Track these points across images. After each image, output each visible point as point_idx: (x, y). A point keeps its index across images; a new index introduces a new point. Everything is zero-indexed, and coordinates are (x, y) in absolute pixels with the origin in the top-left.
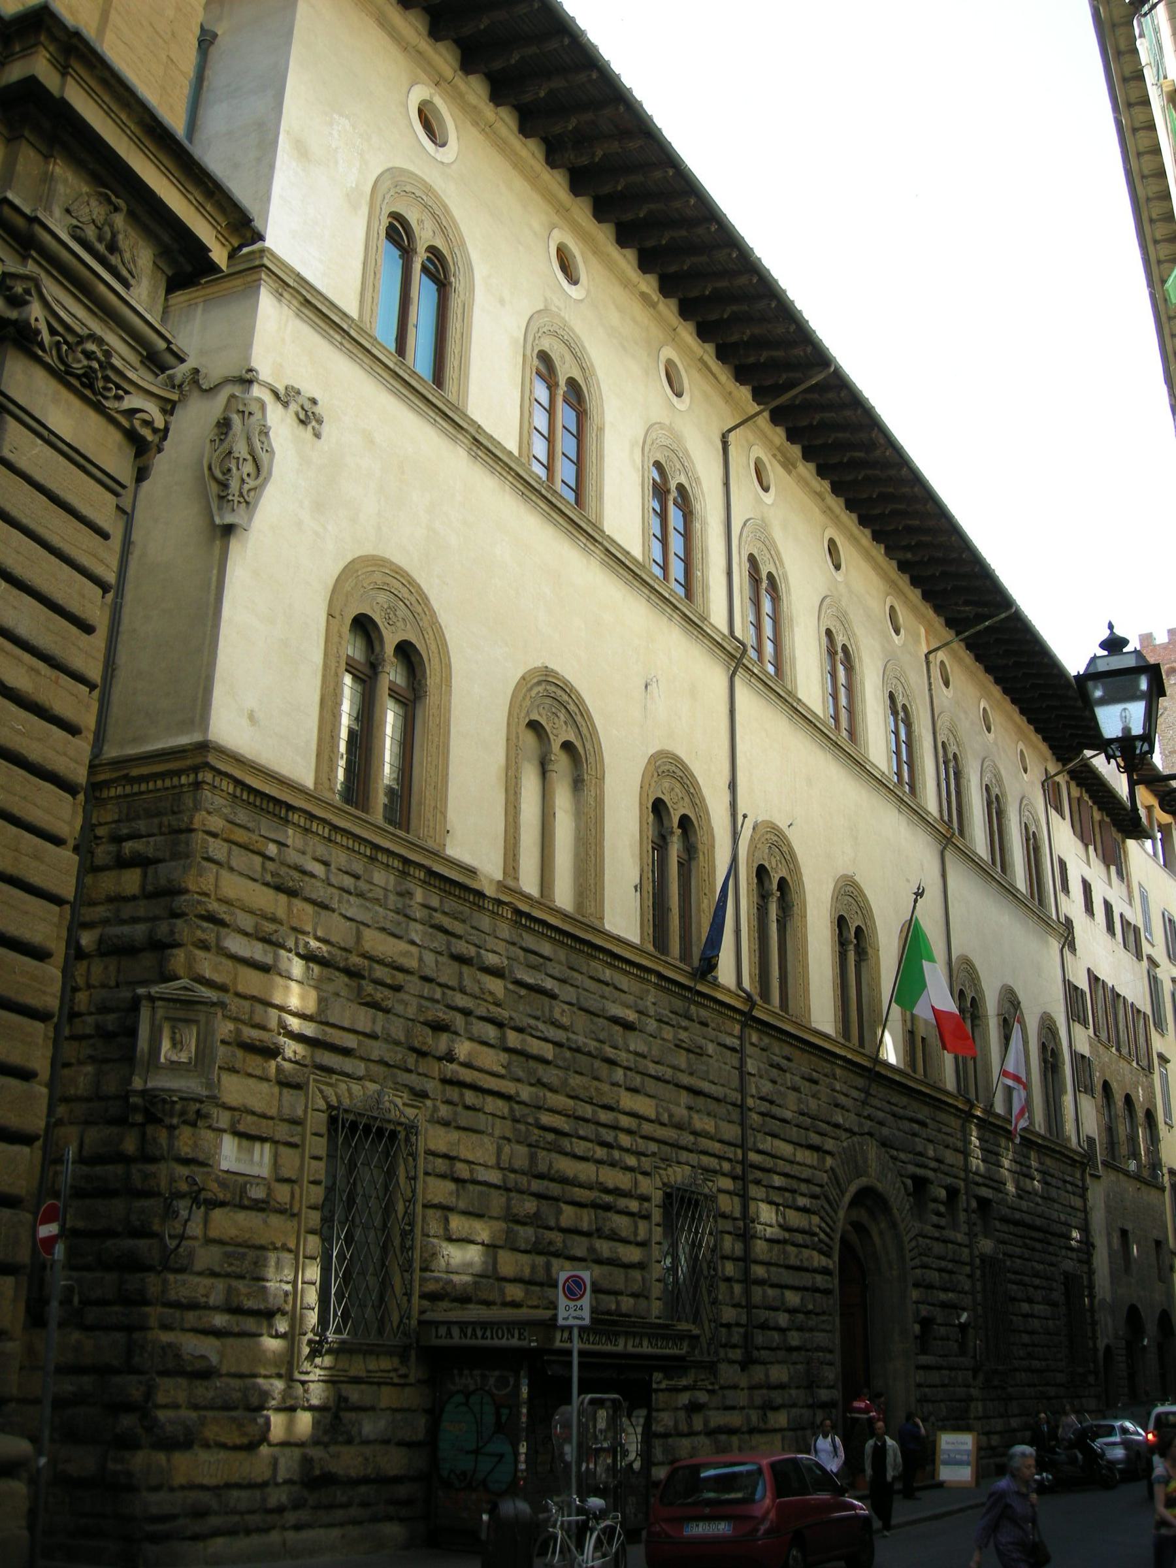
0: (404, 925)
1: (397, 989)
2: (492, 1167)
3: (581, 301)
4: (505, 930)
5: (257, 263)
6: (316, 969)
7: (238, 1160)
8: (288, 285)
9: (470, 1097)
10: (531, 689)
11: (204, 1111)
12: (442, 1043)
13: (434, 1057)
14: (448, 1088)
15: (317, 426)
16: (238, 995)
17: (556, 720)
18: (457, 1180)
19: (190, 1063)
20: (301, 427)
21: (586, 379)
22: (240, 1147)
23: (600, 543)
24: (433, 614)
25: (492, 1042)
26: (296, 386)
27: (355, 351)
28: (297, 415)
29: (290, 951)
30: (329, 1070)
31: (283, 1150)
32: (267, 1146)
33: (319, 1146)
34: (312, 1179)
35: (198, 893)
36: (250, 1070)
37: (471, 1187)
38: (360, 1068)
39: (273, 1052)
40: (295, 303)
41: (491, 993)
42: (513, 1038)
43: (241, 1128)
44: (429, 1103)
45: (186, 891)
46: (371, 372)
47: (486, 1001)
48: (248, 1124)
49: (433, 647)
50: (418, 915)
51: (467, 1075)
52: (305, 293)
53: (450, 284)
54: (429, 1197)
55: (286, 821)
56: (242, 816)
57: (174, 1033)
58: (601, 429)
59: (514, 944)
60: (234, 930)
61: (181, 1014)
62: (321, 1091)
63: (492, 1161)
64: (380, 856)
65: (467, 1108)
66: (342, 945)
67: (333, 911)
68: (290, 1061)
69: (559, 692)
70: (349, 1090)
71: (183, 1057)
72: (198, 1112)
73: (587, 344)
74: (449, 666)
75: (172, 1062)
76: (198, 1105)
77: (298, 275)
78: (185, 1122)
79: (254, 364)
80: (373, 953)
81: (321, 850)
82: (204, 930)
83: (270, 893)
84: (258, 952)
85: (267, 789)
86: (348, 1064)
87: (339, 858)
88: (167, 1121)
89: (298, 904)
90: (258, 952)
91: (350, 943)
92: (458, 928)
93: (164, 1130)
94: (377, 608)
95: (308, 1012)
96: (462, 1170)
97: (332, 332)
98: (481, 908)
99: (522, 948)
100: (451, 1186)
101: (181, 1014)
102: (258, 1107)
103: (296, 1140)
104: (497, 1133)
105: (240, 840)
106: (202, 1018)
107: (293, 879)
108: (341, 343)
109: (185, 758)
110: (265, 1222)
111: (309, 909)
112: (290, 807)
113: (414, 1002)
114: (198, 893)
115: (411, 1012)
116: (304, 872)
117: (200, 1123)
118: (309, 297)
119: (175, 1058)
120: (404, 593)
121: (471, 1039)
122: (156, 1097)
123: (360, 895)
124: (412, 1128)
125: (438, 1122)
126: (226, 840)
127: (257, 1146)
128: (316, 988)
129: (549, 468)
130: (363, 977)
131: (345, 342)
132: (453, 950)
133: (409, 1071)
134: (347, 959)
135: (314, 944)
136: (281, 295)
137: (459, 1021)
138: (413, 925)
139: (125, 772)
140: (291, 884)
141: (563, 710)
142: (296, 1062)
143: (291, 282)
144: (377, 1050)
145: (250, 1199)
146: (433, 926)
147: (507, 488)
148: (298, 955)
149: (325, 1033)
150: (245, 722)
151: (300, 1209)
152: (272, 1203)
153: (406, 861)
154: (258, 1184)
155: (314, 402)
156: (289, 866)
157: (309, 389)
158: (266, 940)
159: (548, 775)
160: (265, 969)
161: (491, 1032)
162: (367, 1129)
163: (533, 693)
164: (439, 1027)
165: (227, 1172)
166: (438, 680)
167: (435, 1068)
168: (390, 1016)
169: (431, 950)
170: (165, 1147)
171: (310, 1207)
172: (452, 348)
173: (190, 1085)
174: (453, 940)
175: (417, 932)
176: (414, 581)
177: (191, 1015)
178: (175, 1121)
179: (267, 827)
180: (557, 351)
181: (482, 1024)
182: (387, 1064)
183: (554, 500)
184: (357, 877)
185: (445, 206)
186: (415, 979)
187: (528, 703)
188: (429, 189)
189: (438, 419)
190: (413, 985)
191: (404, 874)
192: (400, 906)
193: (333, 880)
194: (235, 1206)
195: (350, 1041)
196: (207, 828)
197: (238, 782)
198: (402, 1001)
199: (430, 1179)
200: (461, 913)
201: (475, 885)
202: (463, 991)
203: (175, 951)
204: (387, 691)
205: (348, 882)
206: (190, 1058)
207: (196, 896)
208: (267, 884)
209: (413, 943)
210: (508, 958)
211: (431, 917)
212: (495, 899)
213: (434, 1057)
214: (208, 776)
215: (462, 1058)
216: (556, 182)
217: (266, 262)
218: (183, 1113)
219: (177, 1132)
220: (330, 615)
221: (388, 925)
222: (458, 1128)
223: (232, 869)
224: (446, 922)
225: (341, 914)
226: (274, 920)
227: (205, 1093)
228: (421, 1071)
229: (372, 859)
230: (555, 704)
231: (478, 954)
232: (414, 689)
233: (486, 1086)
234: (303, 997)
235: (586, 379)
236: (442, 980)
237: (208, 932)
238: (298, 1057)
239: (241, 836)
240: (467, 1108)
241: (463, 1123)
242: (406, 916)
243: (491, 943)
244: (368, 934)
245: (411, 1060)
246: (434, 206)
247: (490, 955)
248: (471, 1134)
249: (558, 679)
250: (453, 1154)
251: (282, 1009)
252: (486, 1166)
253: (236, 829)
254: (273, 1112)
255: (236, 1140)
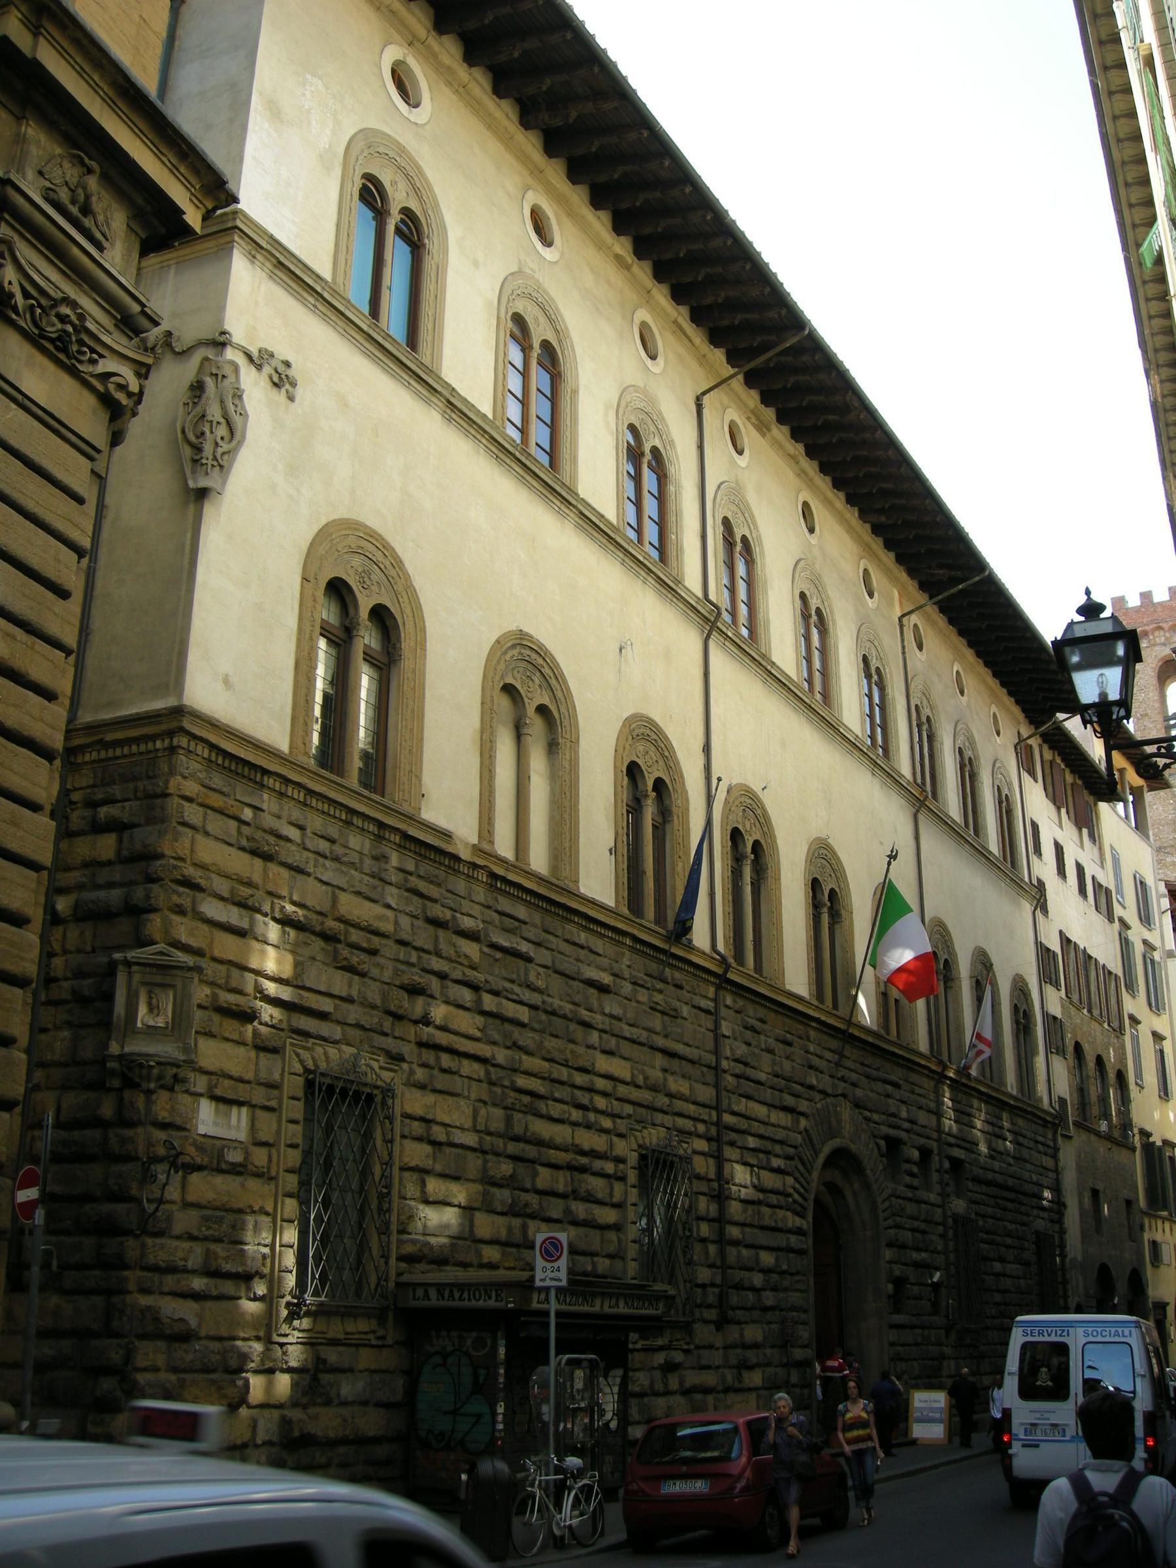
0: (379, 889)
1: (373, 952)
2: (468, 1130)
3: (556, 262)
4: (480, 893)
5: (230, 225)
6: (292, 933)
7: (215, 1124)
8: (262, 248)
9: (446, 1060)
10: (505, 653)
11: (181, 1075)
12: (418, 1006)
13: (410, 1020)
14: (424, 1050)
15: (290, 389)
16: (214, 959)
17: (531, 684)
18: (434, 1143)
19: (167, 1028)
20: (275, 390)
21: (560, 341)
22: (217, 1111)
23: (574, 507)
24: (408, 577)
25: (468, 1005)
26: (270, 349)
27: (329, 313)
28: (271, 378)
29: (266, 915)
30: (306, 1034)
31: (260, 1114)
32: (244, 1110)
33: (296, 1109)
34: (289, 1142)
35: (173, 858)
36: (227, 1035)
37: (448, 1150)
38: (337, 1032)
39: (249, 1016)
40: (268, 264)
41: (466, 956)
42: (489, 1003)
43: (218, 1092)
44: (405, 1066)
45: (161, 856)
46: (344, 334)
47: (461, 964)
48: (225, 1088)
49: (408, 611)
50: (394, 879)
51: (443, 1038)
52: (278, 255)
53: (424, 246)
54: (406, 1160)
55: (262, 786)
56: (217, 781)
57: (151, 998)
58: (575, 392)
59: (489, 907)
60: (210, 895)
61: (158, 979)
62: (298, 1055)
63: (468, 1124)
64: (355, 820)
65: (444, 1071)
66: (318, 908)
67: (309, 875)
68: (266, 1025)
69: (534, 656)
70: (326, 1053)
71: (160, 1022)
72: (175, 1076)
73: (561, 307)
74: (424, 629)
75: (149, 1027)
76: (175, 1070)
77: (271, 237)
78: (162, 1087)
79: (227, 327)
80: (349, 917)
81: (296, 814)
82: (180, 895)
83: (246, 857)
84: (233, 916)
85: (242, 754)
86: (324, 1028)
87: (315, 822)
88: (144, 1085)
89: (274, 868)
90: (233, 916)
91: (326, 907)
92: (433, 891)
93: (142, 1095)
94: (352, 572)
95: (285, 976)
96: (439, 1133)
97: (305, 295)
98: (457, 872)
99: (497, 911)
100: (428, 1149)
101: (158, 979)
102: (235, 1071)
103: (273, 1103)
104: (473, 1096)
105: (216, 805)
106: (179, 983)
107: (268, 843)
108: (314, 306)
109: (159, 723)
110: (243, 1185)
111: (285, 873)
112: (265, 772)
113: (390, 965)
114: (173, 858)
115: (387, 975)
116: (279, 837)
117: (177, 1088)
118: (282, 259)
119: (151, 1023)
120: (379, 556)
121: (447, 1002)
122: (133, 1061)
123: (336, 859)
124: (388, 1091)
125: (415, 1086)
126: (201, 805)
127: (235, 1110)
128: (292, 952)
129: (523, 431)
130: (339, 941)
131: (318, 304)
132: (429, 914)
133: (385, 1034)
134: (323, 923)
135: (290, 908)
136: (254, 257)
137: (435, 984)
138: (389, 889)
139: (100, 737)
140: (266, 848)
141: (538, 674)
142: (272, 1026)
143: (264, 244)
144: (354, 1013)
145: (227, 1162)
146: (408, 890)
147: (482, 452)
148: (274, 919)
149: (302, 997)
150: (220, 686)
151: (278, 1172)
152: (250, 1167)
153: (381, 825)
154: (235, 1148)
155: (287, 364)
156: (265, 831)
157: (283, 351)
158: (242, 905)
159: (523, 738)
160: (241, 933)
161: (467, 995)
162: (344, 1093)
163: (508, 657)
164: (414, 991)
165: (205, 1136)
166: (412, 644)
167: (411, 1031)
168: (366, 980)
169: (407, 914)
170: (143, 1112)
171: (287, 1171)
172: (426, 309)
173: (168, 1049)
174: (429, 904)
175: (392, 896)
176: (388, 544)
177: (168, 980)
178: (152, 1085)
179: (242, 791)
180: (531, 314)
181: (457, 987)
182: (362, 1028)
183: (528, 463)
184: (332, 841)
185: (419, 167)
186: (391, 943)
187: (502, 666)
188: (402, 150)
189: (412, 382)
190: (389, 949)
191: (379, 838)
192: (375, 870)
193: (309, 845)
194: (213, 1170)
195: (326, 1005)
196: (182, 793)
197: (213, 747)
198: (378, 965)
199: (407, 1142)
200: (436, 876)
201: (450, 849)
202: (438, 954)
203: (152, 916)
204: (362, 655)
205: (324, 846)
206: (167, 1023)
207: (172, 861)
208: (242, 849)
209: (388, 907)
210: (483, 922)
211: (406, 880)
212: (470, 863)
213: (410, 1020)
214: (184, 741)
215: (438, 1022)
216: (530, 143)
217: (239, 223)
218: (160, 1077)
219: (154, 1097)
220: (305, 579)
221: (364, 889)
222: (434, 1091)
223: (207, 834)
224: (422, 886)
225: (317, 878)
226: (249, 884)
227: (182, 1057)
228: (397, 1034)
229: (348, 823)
230: (530, 667)
231: (454, 917)
232: (388, 653)
233: (462, 1049)
234: (279, 962)
235: (560, 341)
236: (418, 944)
237: (184, 897)
238: (274, 1021)
239: (216, 800)
240: (444, 1071)
241: (439, 1086)
242: (381, 880)
243: (466, 906)
244: (344, 898)
245: (387, 1023)
246: (408, 167)
247: (466, 918)
248: (448, 1097)
249: (533, 642)
250: (430, 1117)
251: (258, 973)
252: (462, 1129)
253: (211, 794)
254: (249, 1076)
255: (213, 1103)
